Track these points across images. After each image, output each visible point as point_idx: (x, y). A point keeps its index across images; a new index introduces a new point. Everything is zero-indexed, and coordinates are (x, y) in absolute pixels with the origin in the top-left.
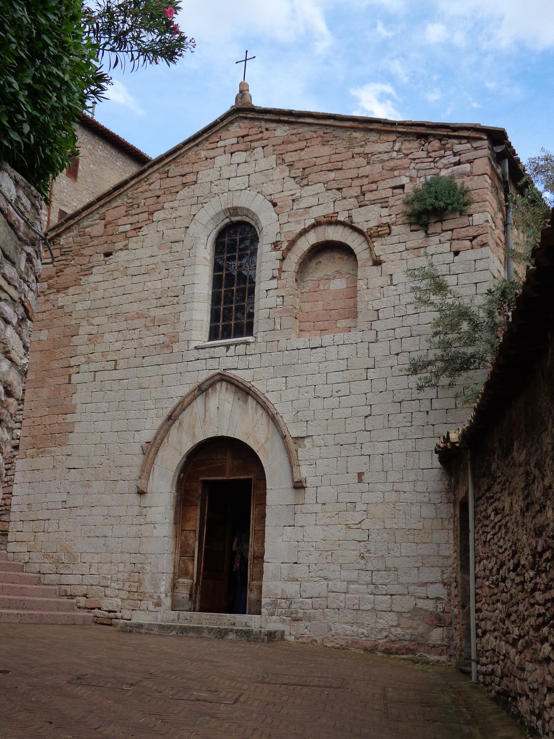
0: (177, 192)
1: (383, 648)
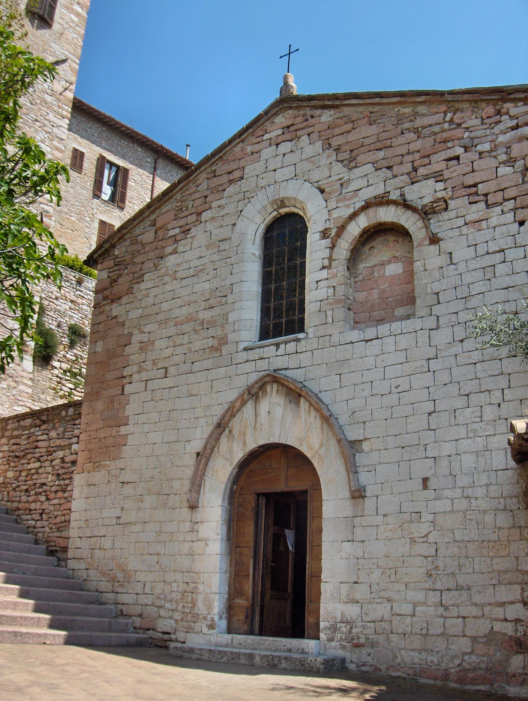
0: (224, 190)
1: (456, 678)
